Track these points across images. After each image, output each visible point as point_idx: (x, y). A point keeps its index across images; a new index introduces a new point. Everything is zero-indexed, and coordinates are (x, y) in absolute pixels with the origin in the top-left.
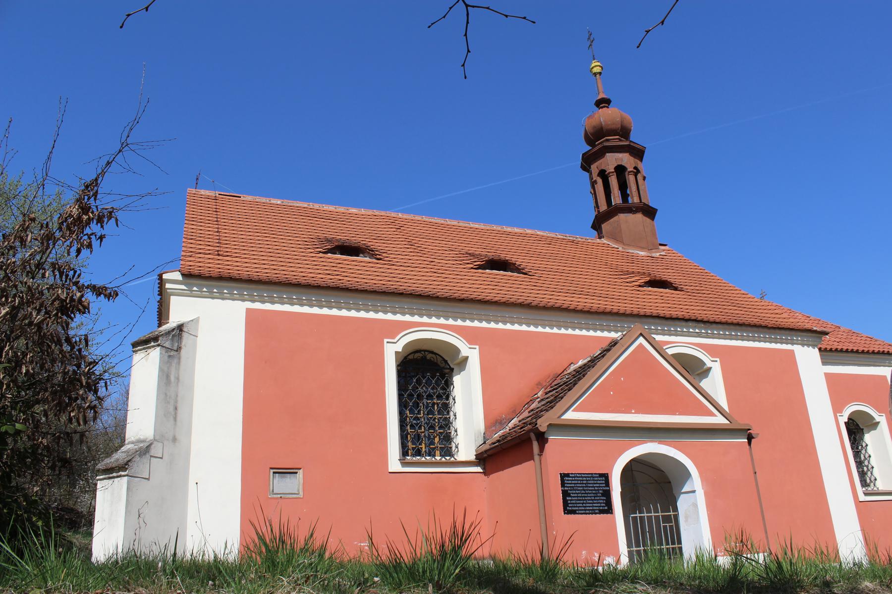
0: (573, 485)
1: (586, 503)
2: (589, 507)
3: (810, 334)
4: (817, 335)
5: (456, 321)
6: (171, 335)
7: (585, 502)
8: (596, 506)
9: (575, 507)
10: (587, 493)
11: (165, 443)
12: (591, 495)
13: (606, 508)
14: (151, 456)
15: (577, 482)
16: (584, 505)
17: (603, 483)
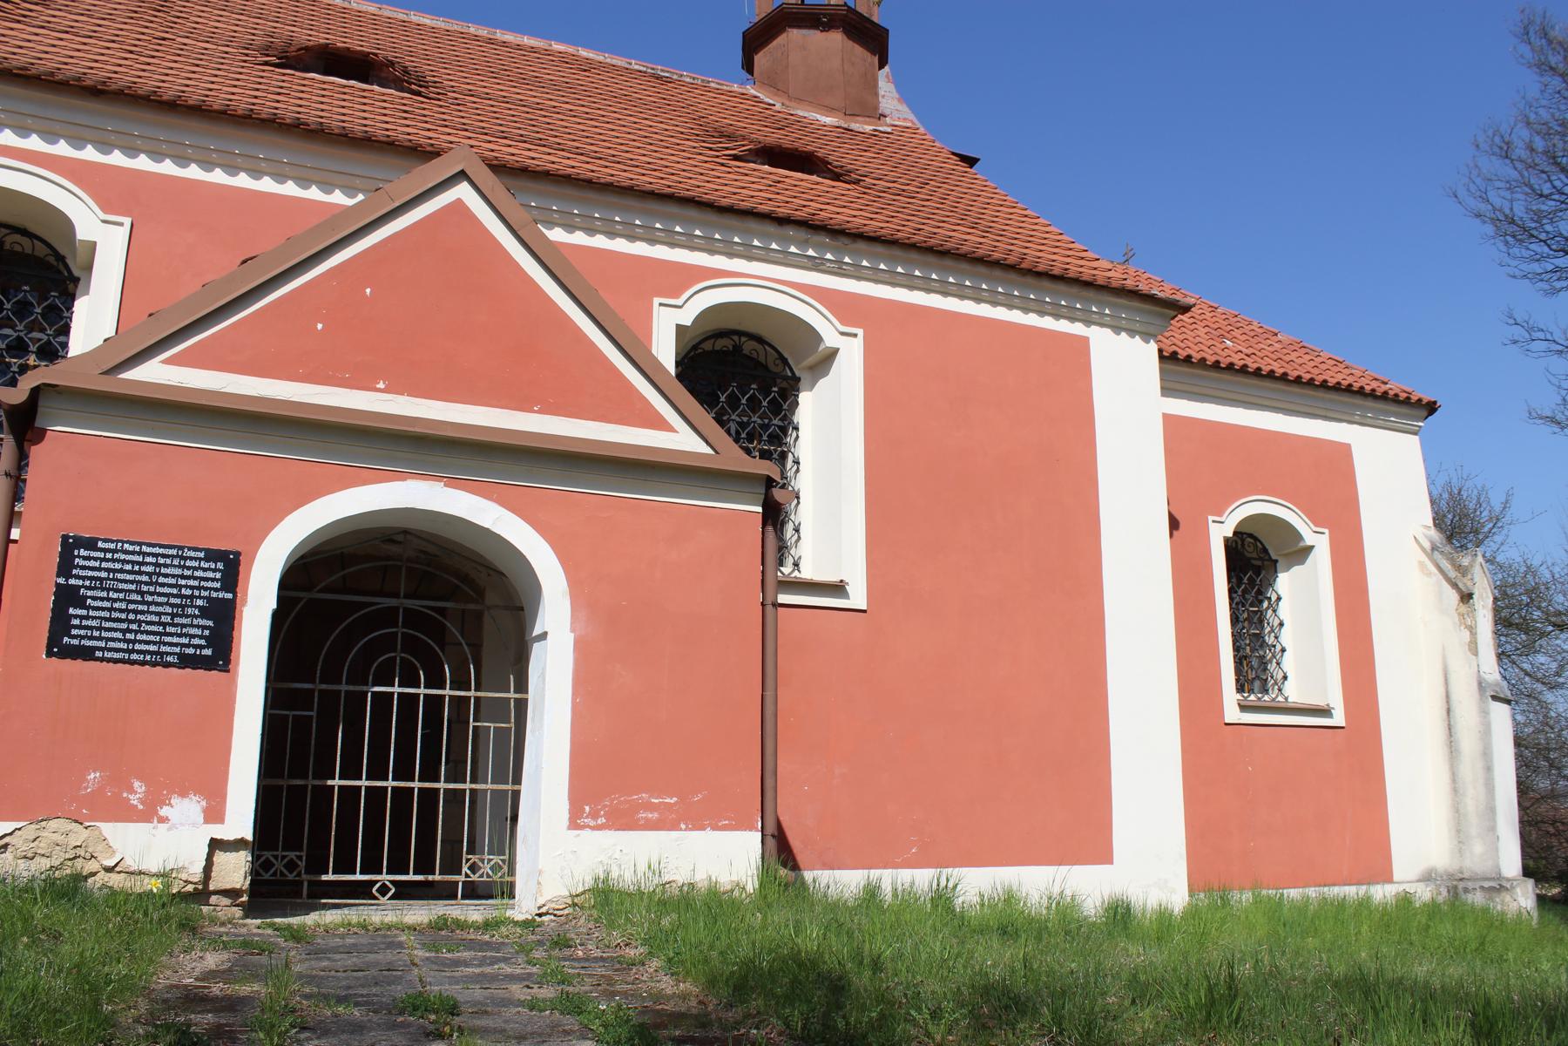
0: (104, 574)
1: (136, 632)
3: (1137, 304)
4: (1158, 309)
7: (134, 627)
8: (171, 644)
9: (92, 638)
10: (149, 604)
12: (160, 609)
13: (208, 652)
15: (118, 566)
17: (213, 580)
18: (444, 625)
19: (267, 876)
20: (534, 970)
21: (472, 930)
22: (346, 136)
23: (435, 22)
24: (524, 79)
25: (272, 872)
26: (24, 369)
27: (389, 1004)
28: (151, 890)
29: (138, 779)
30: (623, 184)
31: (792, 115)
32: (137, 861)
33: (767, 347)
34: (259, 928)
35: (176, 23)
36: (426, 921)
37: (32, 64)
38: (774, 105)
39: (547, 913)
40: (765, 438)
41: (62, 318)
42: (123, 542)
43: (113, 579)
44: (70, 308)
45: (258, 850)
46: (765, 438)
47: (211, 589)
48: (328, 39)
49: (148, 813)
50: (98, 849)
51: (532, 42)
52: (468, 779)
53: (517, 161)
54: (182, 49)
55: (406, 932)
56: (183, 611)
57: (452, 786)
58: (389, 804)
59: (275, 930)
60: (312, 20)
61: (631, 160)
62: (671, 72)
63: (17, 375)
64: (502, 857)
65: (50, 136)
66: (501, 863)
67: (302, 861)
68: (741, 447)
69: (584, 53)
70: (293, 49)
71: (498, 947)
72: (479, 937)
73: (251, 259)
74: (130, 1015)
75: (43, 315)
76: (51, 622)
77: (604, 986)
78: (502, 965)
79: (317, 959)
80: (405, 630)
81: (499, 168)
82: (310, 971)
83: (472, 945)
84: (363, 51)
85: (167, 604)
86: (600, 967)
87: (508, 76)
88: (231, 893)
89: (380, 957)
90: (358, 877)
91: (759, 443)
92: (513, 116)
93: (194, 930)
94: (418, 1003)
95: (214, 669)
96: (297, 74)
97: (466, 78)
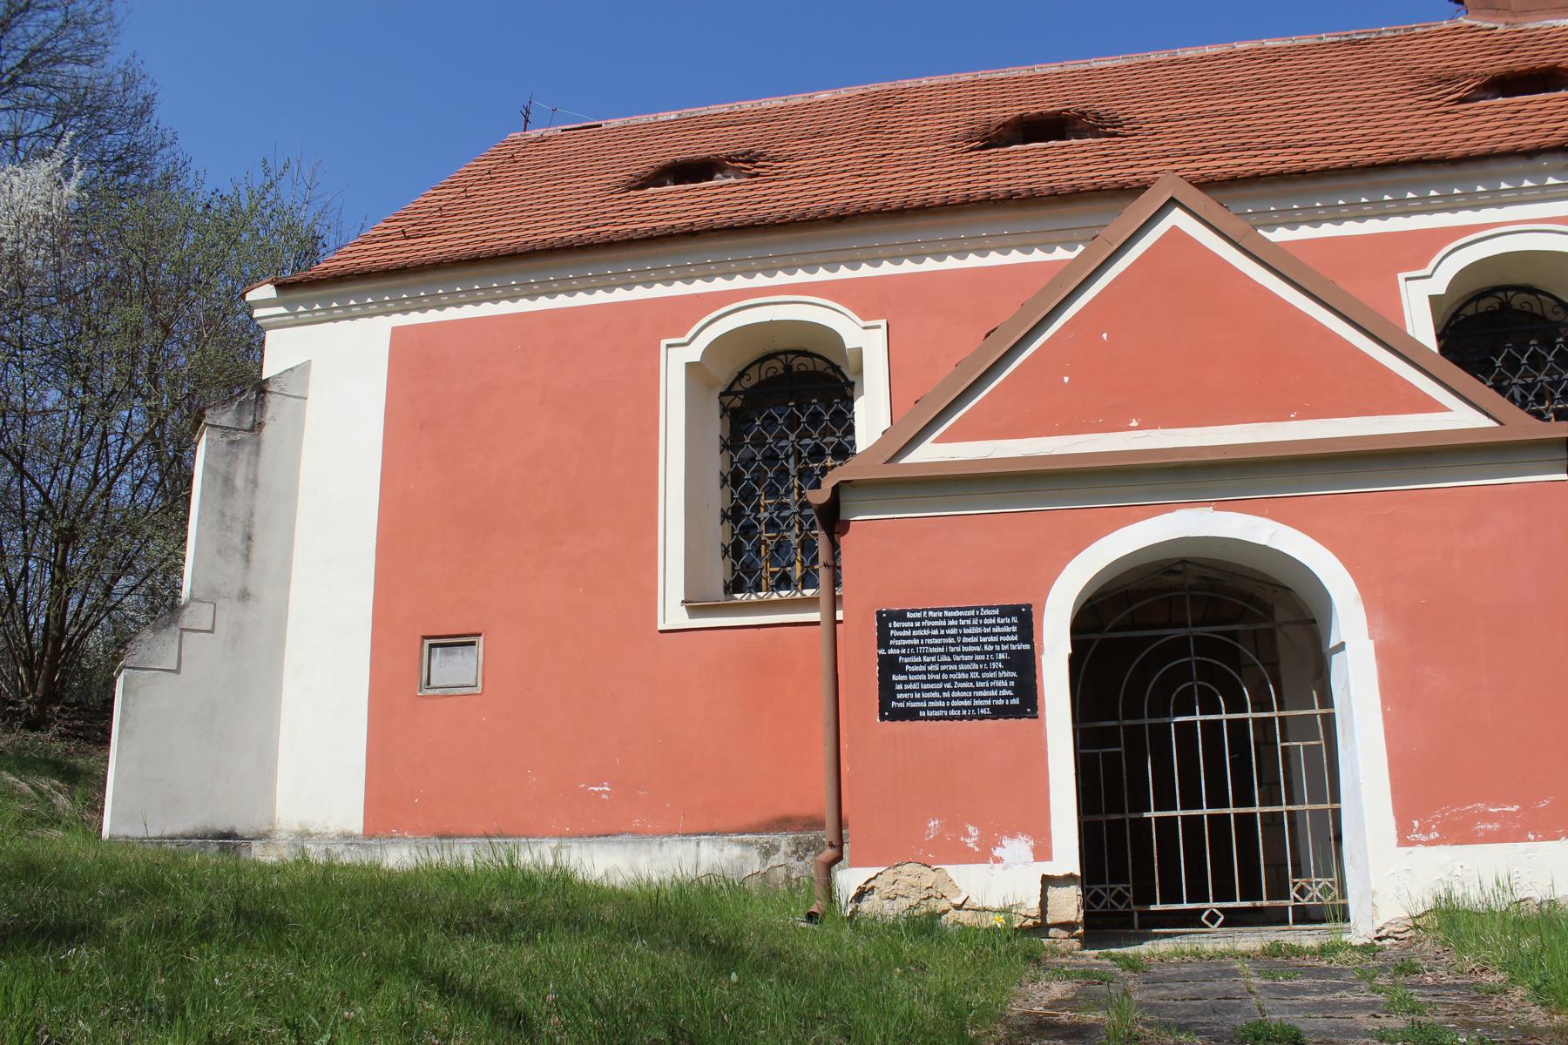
0: (916, 642)
1: (951, 690)
2: (962, 699)
5: (814, 272)
6: (236, 403)
7: (948, 686)
8: (982, 698)
9: (914, 700)
10: (958, 663)
11: (220, 603)
12: (968, 667)
13: (1016, 701)
14: (183, 630)
15: (926, 632)
16: (946, 695)
17: (1011, 634)
18: (1237, 648)
19: (1098, 909)
20: (1380, 998)
21: (1308, 956)
22: (1055, 194)
23: (1115, 61)
24: (1214, 89)
25: (1102, 904)
26: (824, 470)
27: (1230, 1033)
28: (996, 925)
29: (971, 825)
30: (1340, 165)
31: (1520, 32)
32: (980, 897)
33: (1540, 296)
34: (1097, 958)
35: (890, 139)
36: (1259, 948)
37: (789, 211)
38: (1496, 28)
39: (1387, 937)
40: (1558, 396)
41: (846, 420)
42: (927, 610)
43: (925, 645)
44: (851, 410)
45: (1087, 883)
46: (1558, 396)
47: (1009, 642)
48: (1021, 110)
49: (984, 855)
50: (946, 890)
51: (1214, 49)
52: (1284, 801)
53: (1225, 173)
54: (900, 160)
55: (1240, 959)
56: (988, 666)
57: (1267, 809)
58: (1206, 832)
59: (1112, 960)
60: (1049, 93)
61: (1343, 137)
62: (1368, 33)
63: (820, 477)
64: (1330, 879)
65: (811, 268)
66: (1329, 885)
67: (1129, 892)
68: (1530, 412)
69: (1269, 44)
70: (992, 128)
71: (1338, 973)
72: (1316, 964)
73: (993, 331)
74: (991, 1039)
75: (831, 420)
76: (879, 689)
77: (1461, 1017)
78: (1344, 993)
79: (1154, 988)
80: (1198, 658)
81: (1206, 185)
82: (1149, 1000)
83: (1310, 972)
84: (1055, 111)
85: (973, 661)
86: (1454, 995)
87: (1198, 91)
88: (1068, 926)
89: (1216, 985)
90: (1186, 906)
91: (1552, 402)
92: (1211, 129)
93: (1038, 961)
94: (1259, 1032)
95: (1025, 717)
96: (1001, 150)
97: (1157, 106)
